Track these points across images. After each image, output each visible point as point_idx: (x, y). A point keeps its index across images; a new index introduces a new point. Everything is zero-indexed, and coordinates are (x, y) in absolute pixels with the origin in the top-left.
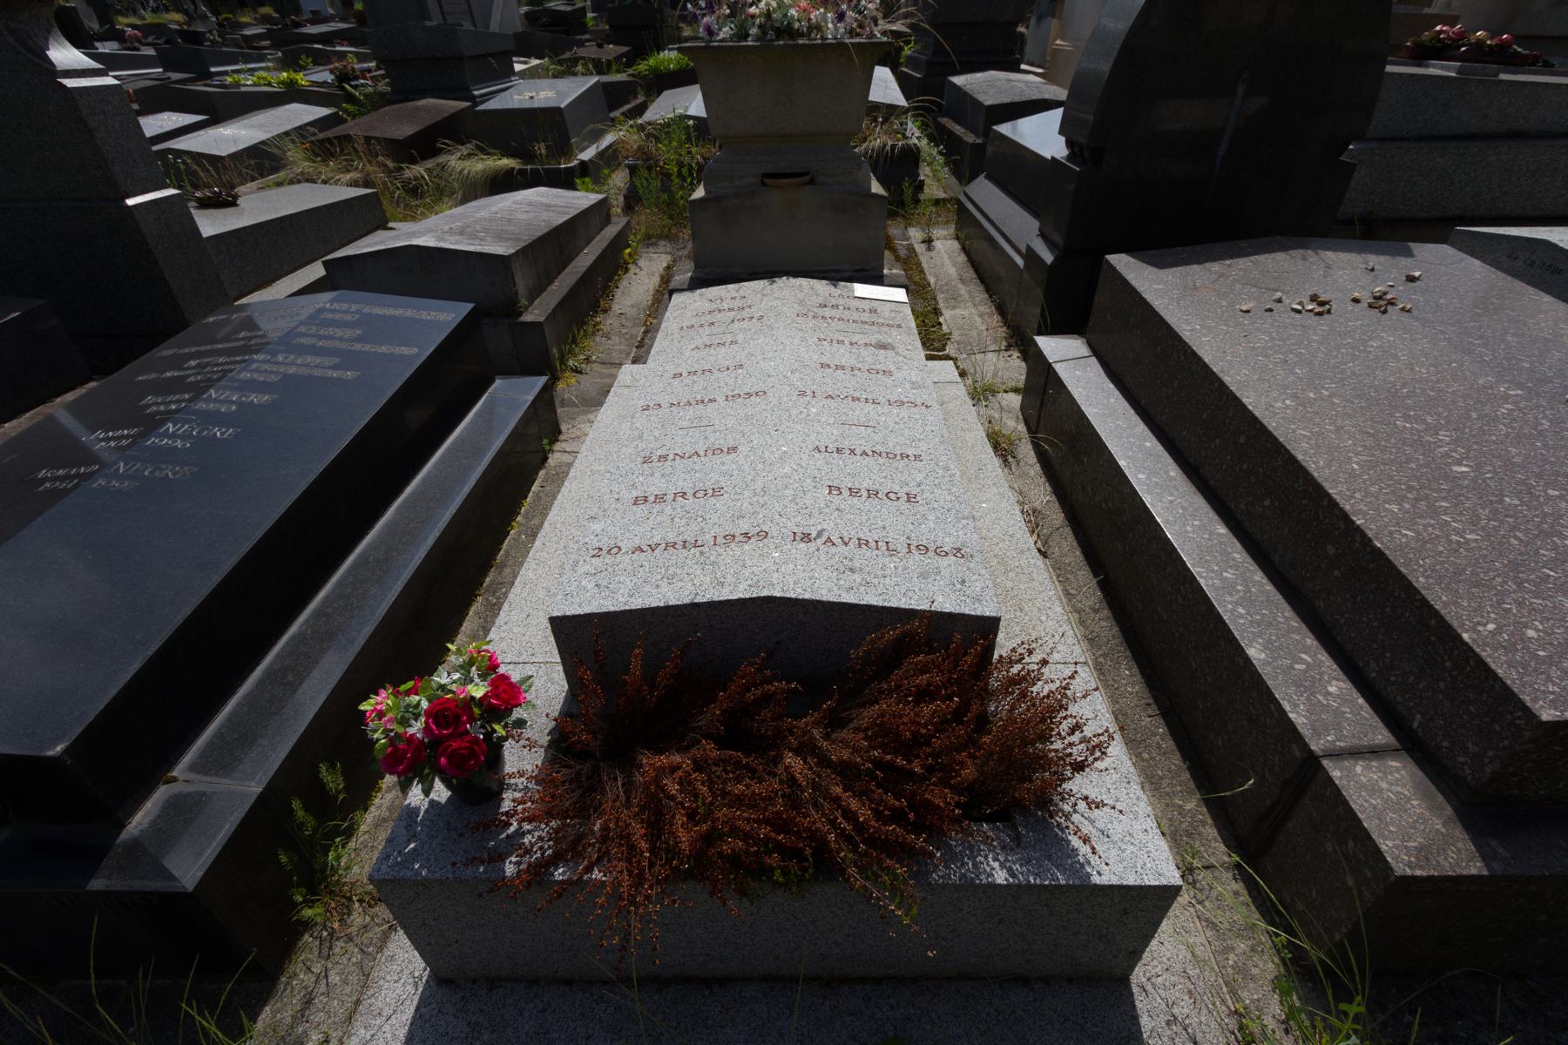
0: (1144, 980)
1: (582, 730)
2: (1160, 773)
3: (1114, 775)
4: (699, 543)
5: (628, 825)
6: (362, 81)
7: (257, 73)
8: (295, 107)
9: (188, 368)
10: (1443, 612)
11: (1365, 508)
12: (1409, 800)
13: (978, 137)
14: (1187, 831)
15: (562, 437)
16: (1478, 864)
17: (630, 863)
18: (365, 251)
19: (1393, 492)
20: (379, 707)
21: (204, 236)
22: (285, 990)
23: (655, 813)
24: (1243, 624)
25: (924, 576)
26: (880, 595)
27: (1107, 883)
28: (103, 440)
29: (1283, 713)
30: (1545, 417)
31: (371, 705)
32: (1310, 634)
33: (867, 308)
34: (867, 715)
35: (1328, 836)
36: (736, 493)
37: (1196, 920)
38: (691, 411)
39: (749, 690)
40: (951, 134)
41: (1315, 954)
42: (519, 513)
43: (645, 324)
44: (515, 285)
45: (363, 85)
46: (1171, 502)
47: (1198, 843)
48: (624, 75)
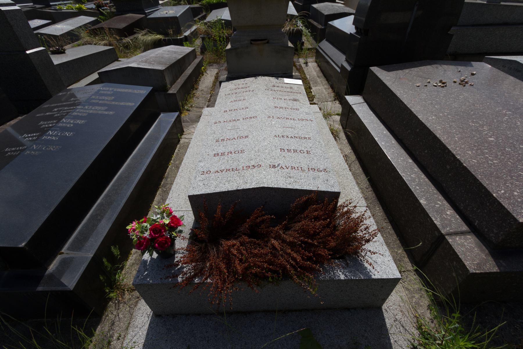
0: (386, 308)
1: (202, 233)
2: (390, 241)
3: (378, 243)
4: (238, 169)
5: (219, 264)
6: (106, 8)
7: (67, 5)
8: (82, 17)
9: (54, 112)
10: (487, 187)
11: (460, 153)
12: (474, 248)
13: (322, 26)
14: (399, 260)
15: (184, 133)
16: (496, 268)
17: (221, 277)
18: (112, 69)
19: (469, 147)
20: (133, 228)
21: (55, 64)
22: (105, 320)
23: (228, 259)
24: (418, 192)
25: (314, 178)
26: (300, 185)
27: (377, 278)
28: (27, 137)
29: (433, 221)
30: (519, 121)
31: (131, 227)
32: (440, 195)
33: (289, 87)
34: (298, 226)
35: (447, 260)
36: (249, 152)
37: (403, 288)
38: (231, 124)
39: (257, 219)
40: (313, 25)
41: (442, 297)
42: (171, 160)
43: (210, 94)
44: (166, 80)
45: (106, 9)
46: (393, 152)
47: (402, 263)
48: (198, 5)
